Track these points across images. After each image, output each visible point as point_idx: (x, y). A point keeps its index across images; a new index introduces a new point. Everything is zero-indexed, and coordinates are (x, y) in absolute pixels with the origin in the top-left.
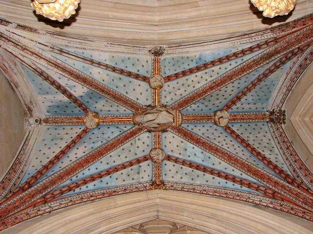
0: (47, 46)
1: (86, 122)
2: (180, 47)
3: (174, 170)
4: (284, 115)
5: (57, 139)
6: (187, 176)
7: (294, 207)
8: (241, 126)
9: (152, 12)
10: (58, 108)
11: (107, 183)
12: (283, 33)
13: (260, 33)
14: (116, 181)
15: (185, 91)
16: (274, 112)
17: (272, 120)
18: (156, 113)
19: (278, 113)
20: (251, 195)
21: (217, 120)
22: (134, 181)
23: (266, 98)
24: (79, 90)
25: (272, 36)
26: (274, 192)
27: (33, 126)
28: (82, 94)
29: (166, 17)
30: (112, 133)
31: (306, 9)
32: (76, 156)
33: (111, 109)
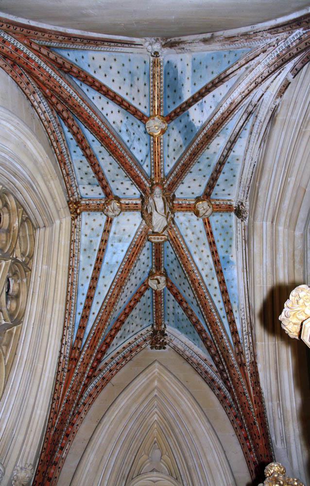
0: (259, 101)
1: (154, 119)
2: (244, 241)
3: (95, 225)
4: (160, 348)
5: (132, 80)
6: (88, 243)
7: (63, 385)
8: (149, 298)
9: (289, 226)
10: (173, 84)
11: (75, 152)
12: (249, 375)
13: (251, 348)
14: (79, 161)
15: (191, 241)
16: (163, 336)
17: (155, 332)
18: (165, 213)
19: (163, 341)
20: (70, 329)
21: (155, 277)
22: (79, 179)
23: (180, 327)
24: (198, 116)
25: (247, 360)
26: (76, 360)
27: (150, 47)
28: (191, 118)
29: (281, 239)
30: (139, 151)
31: (272, 401)
32: (109, 113)
33: (171, 149)
